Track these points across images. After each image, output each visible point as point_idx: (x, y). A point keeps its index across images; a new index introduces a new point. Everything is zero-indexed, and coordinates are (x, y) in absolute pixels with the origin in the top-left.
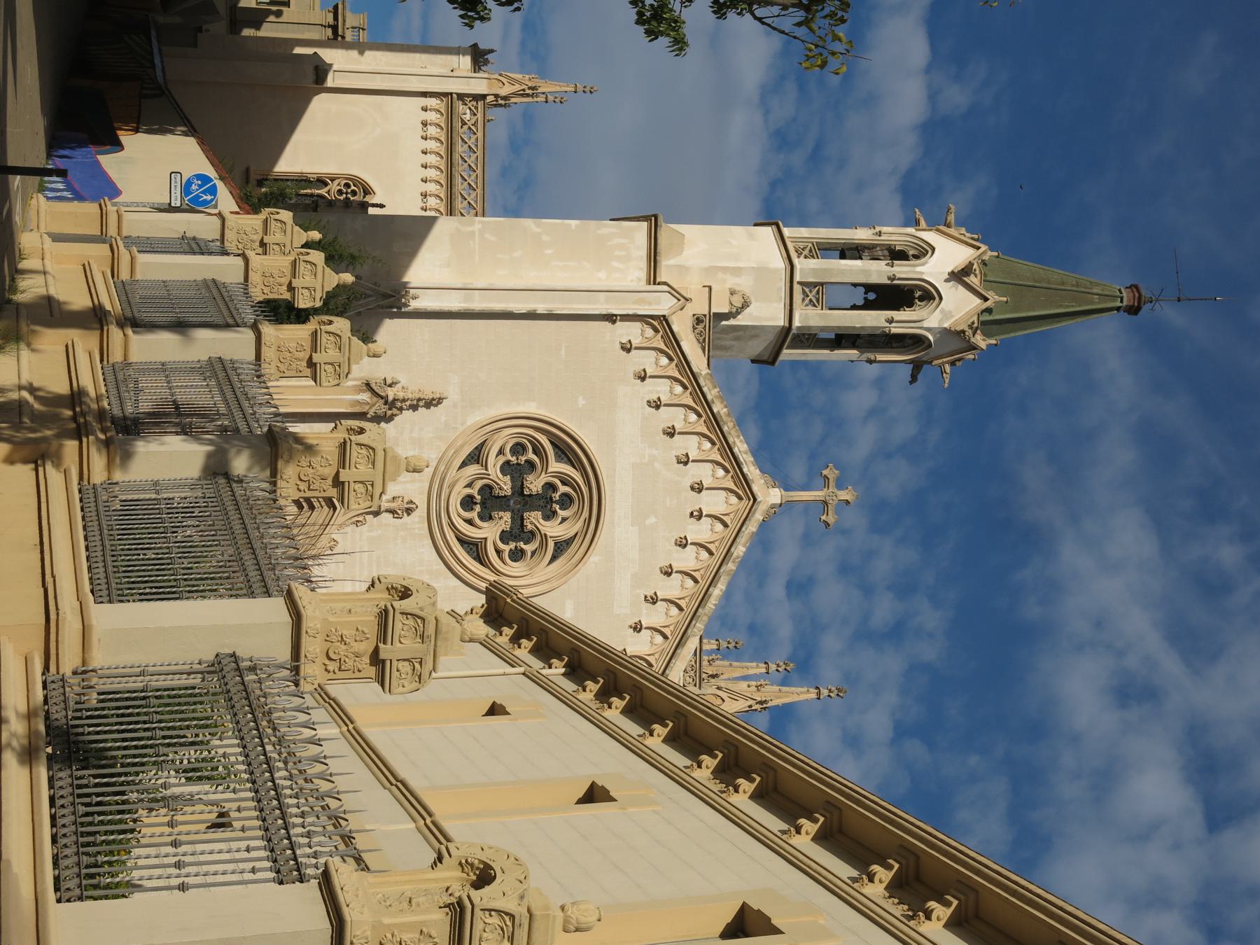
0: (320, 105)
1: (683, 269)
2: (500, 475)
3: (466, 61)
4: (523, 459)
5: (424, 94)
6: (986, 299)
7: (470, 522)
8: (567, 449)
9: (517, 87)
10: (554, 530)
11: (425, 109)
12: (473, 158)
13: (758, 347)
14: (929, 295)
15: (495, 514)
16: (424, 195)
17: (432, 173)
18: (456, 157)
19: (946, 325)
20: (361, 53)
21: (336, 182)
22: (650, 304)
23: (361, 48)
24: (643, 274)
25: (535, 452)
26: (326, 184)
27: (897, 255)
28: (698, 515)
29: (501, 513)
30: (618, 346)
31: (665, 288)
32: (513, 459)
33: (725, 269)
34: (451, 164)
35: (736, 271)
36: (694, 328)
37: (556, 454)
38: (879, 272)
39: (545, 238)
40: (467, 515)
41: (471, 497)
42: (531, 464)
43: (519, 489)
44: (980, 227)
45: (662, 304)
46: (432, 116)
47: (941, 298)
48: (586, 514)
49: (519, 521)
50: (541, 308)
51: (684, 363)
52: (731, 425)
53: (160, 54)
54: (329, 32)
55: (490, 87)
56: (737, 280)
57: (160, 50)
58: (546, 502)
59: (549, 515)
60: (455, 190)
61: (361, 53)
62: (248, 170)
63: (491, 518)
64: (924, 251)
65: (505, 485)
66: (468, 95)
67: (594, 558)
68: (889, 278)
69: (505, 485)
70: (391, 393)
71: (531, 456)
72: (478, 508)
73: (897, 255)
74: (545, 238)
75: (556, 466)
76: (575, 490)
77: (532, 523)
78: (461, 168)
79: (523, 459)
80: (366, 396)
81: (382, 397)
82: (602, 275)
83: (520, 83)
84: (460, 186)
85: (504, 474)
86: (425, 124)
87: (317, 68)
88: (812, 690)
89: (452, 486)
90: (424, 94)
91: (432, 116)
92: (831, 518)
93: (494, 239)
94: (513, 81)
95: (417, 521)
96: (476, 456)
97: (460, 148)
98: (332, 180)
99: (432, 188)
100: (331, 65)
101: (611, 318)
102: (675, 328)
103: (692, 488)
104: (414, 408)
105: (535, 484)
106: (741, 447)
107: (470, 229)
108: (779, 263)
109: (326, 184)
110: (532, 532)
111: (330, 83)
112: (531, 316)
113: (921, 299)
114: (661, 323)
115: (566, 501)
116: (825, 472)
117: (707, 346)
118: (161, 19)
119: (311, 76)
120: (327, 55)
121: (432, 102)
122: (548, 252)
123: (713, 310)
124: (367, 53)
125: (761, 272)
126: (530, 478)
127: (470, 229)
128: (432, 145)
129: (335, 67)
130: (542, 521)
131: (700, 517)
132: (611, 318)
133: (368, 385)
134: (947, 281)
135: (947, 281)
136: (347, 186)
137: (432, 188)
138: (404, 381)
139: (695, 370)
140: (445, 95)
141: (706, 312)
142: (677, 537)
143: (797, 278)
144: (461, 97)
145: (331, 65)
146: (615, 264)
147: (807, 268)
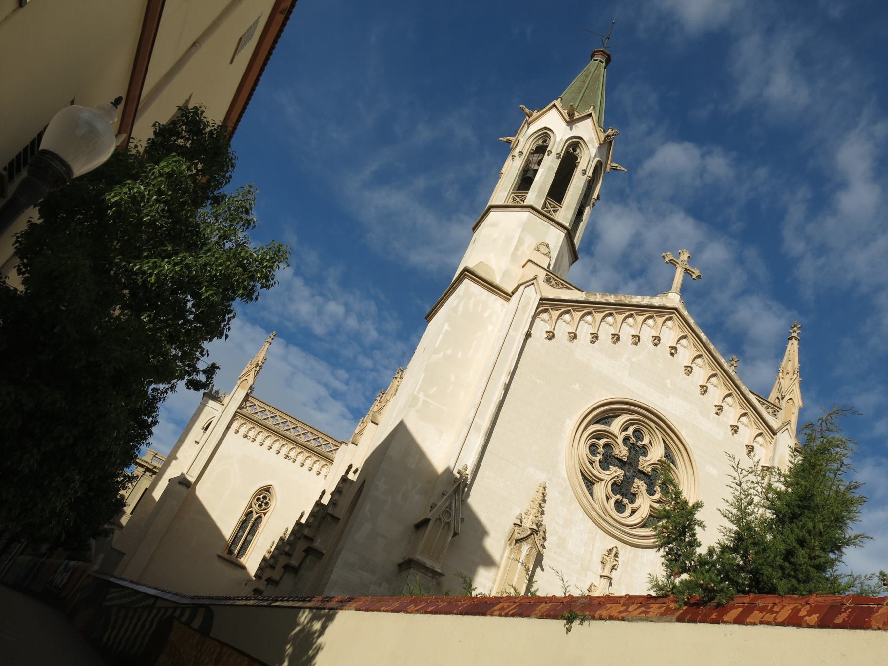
0: (202, 492)
1: (506, 274)
2: (608, 472)
3: (211, 403)
4: (601, 450)
5: (228, 428)
6: (590, 115)
7: (634, 512)
8: (605, 414)
9: (252, 374)
10: (656, 453)
11: (237, 432)
12: (278, 418)
13: (566, 259)
14: (575, 144)
15: (633, 490)
16: (287, 457)
17: (276, 446)
18: (273, 428)
19: (597, 145)
20: (176, 458)
21: (253, 505)
22: (528, 304)
23: (172, 457)
24: (500, 301)
25: (599, 439)
26: (251, 512)
27: (541, 150)
28: (674, 351)
29: (635, 485)
30: (547, 341)
31: (522, 287)
32: (600, 457)
33: (516, 248)
34: (276, 433)
35: (520, 241)
36: (552, 286)
37: (605, 424)
38: (552, 161)
39: (449, 352)
40: (628, 511)
41: (617, 502)
42: (607, 446)
43: (621, 463)
44: (541, 103)
45: (531, 297)
46: (243, 430)
47: (580, 138)
48: (653, 425)
49: (643, 474)
50: (505, 379)
51: (576, 305)
52: (623, 298)
53: (121, 579)
54: (147, 473)
55: (243, 388)
56: (526, 245)
57: (115, 577)
58: (637, 450)
59: (644, 451)
60: (292, 438)
61: (176, 458)
62: (219, 557)
63: (634, 495)
64: (545, 134)
65: (615, 472)
66: (242, 403)
67: (683, 433)
68: (558, 158)
69: (615, 472)
70: (528, 524)
71: (602, 442)
72: (625, 501)
73: (541, 150)
74: (449, 352)
75: (616, 426)
76: (633, 424)
77: (648, 466)
78: (282, 428)
79: (601, 450)
80: (525, 547)
81: (532, 534)
82: (490, 327)
83: (251, 370)
84: (292, 434)
85: (608, 469)
86: (245, 436)
87: (180, 483)
88: (790, 342)
89: (606, 511)
90: (228, 428)
91: (243, 430)
92: (697, 272)
93: (434, 389)
94: (247, 374)
95: (625, 552)
96: (590, 482)
97: (270, 423)
98: (251, 507)
99: (284, 450)
100: (182, 474)
101: (528, 335)
102: (551, 297)
103: (656, 345)
104: (542, 513)
105: (621, 451)
106: (638, 300)
107: (420, 403)
108: (525, 215)
109: (251, 512)
110: (653, 470)
111: (192, 480)
112: (507, 388)
113: (575, 150)
114: (546, 305)
115: (638, 434)
116: (667, 260)
117: (567, 285)
118: (96, 567)
119: (183, 489)
120: (173, 472)
121: (235, 425)
122: (460, 355)
123: (546, 267)
124: (178, 455)
125: (525, 228)
126: (616, 451)
127: (420, 403)
128: (260, 438)
129: (185, 472)
130: (647, 459)
131: (676, 349)
132: (528, 335)
133: (517, 541)
134: (571, 129)
135: (571, 129)
136: (258, 499)
137: (284, 450)
138: (517, 511)
139: (582, 299)
140: (235, 416)
141: (545, 273)
142: (684, 372)
143: (539, 208)
144: (240, 408)
145: (182, 474)
146: (486, 314)
147: (536, 195)
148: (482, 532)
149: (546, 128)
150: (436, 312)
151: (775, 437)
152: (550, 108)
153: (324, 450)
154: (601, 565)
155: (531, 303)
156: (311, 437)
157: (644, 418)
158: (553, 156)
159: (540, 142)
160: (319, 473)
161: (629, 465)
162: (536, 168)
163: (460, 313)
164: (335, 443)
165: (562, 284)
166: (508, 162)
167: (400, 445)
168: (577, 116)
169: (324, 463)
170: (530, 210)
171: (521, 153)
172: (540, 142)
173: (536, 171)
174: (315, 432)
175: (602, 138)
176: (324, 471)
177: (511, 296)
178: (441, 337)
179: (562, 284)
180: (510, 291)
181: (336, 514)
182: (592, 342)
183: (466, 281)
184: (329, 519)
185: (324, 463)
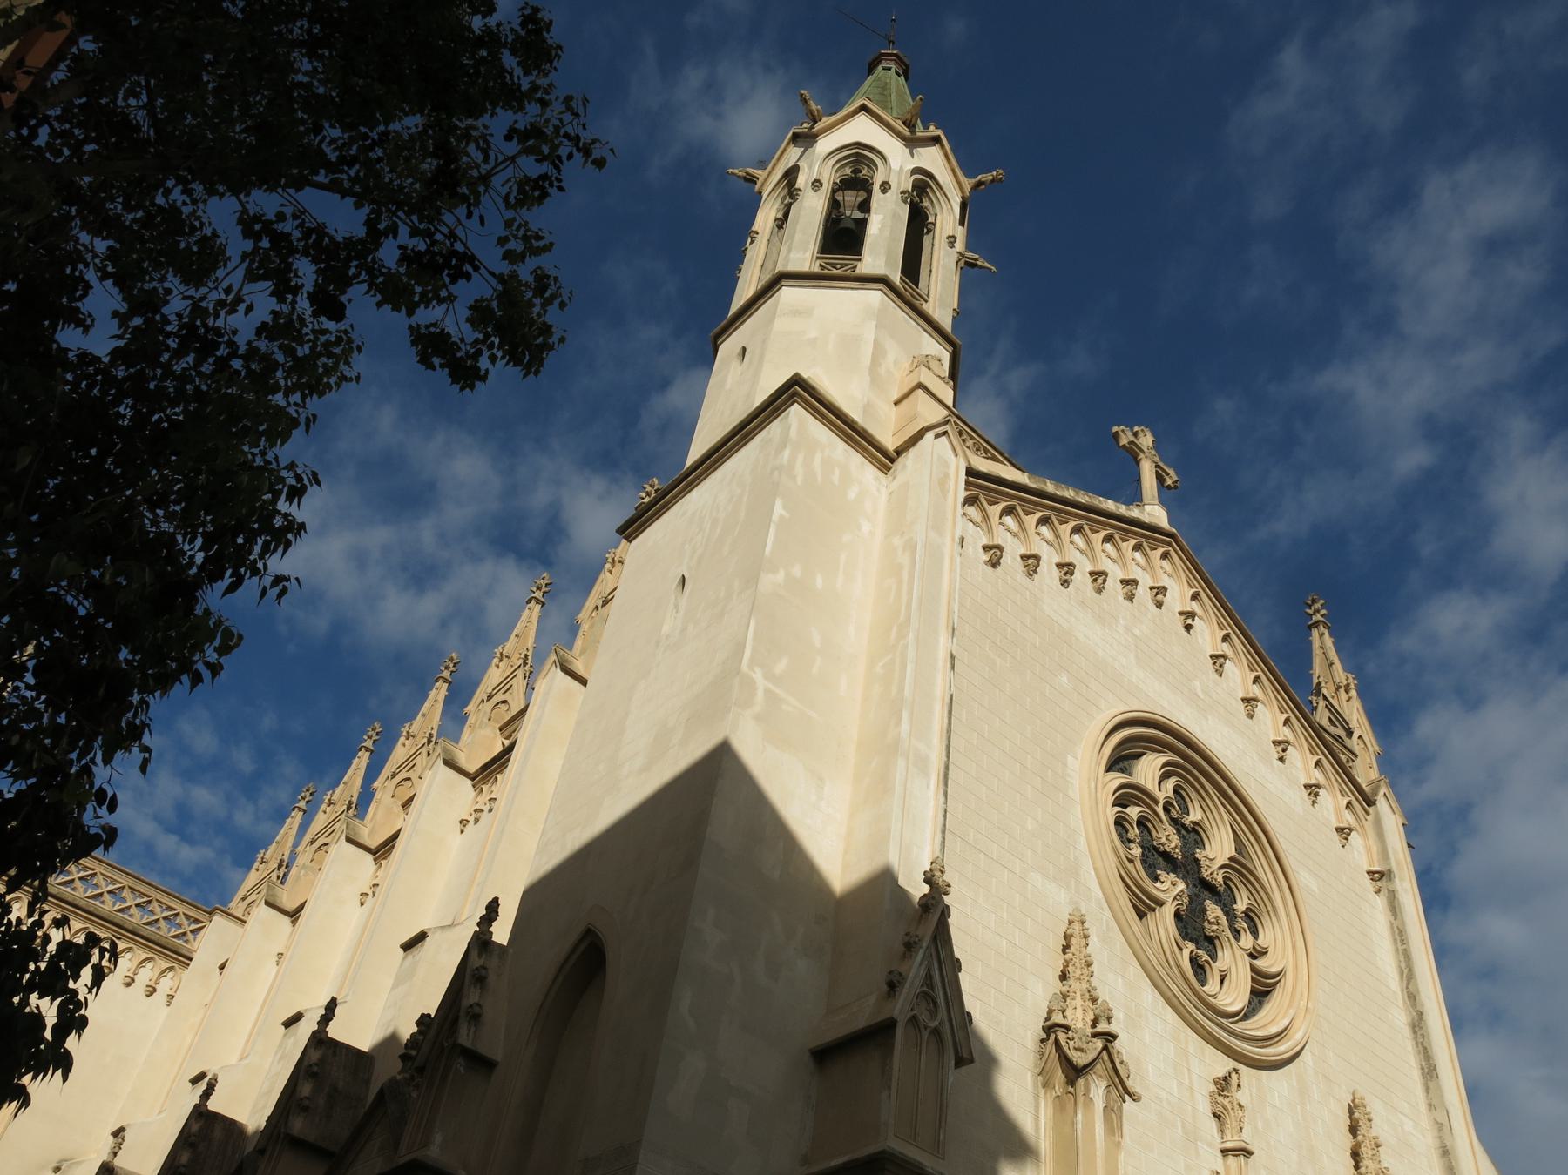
24: (870, 472)
30: (990, 569)
60: (82, 904)
82: (866, 527)
88: (1315, 633)
122: (819, 581)
148: (990, 1061)
149: (858, 145)
150: (666, 507)
151: (1371, 810)
152: (855, 113)
153: (165, 931)
154: (1213, 1123)
155: (952, 476)
156: (131, 900)
157: (1193, 764)
158: (894, 194)
159: (848, 171)
160: (151, 991)
161: (1187, 867)
162: (858, 215)
163: (799, 480)
164: (194, 914)
165: (986, 451)
166: (760, 217)
167: (705, 819)
168: (921, 132)
169: (166, 965)
170: (882, 287)
171: (817, 184)
172: (848, 171)
173: (862, 224)
174: (142, 888)
175: (968, 189)
176: (165, 985)
177: (892, 461)
178: (772, 531)
179: (986, 451)
180: (890, 444)
181: (483, 1049)
182: (1065, 583)
183: (796, 412)
184: (460, 1065)
185: (166, 965)
